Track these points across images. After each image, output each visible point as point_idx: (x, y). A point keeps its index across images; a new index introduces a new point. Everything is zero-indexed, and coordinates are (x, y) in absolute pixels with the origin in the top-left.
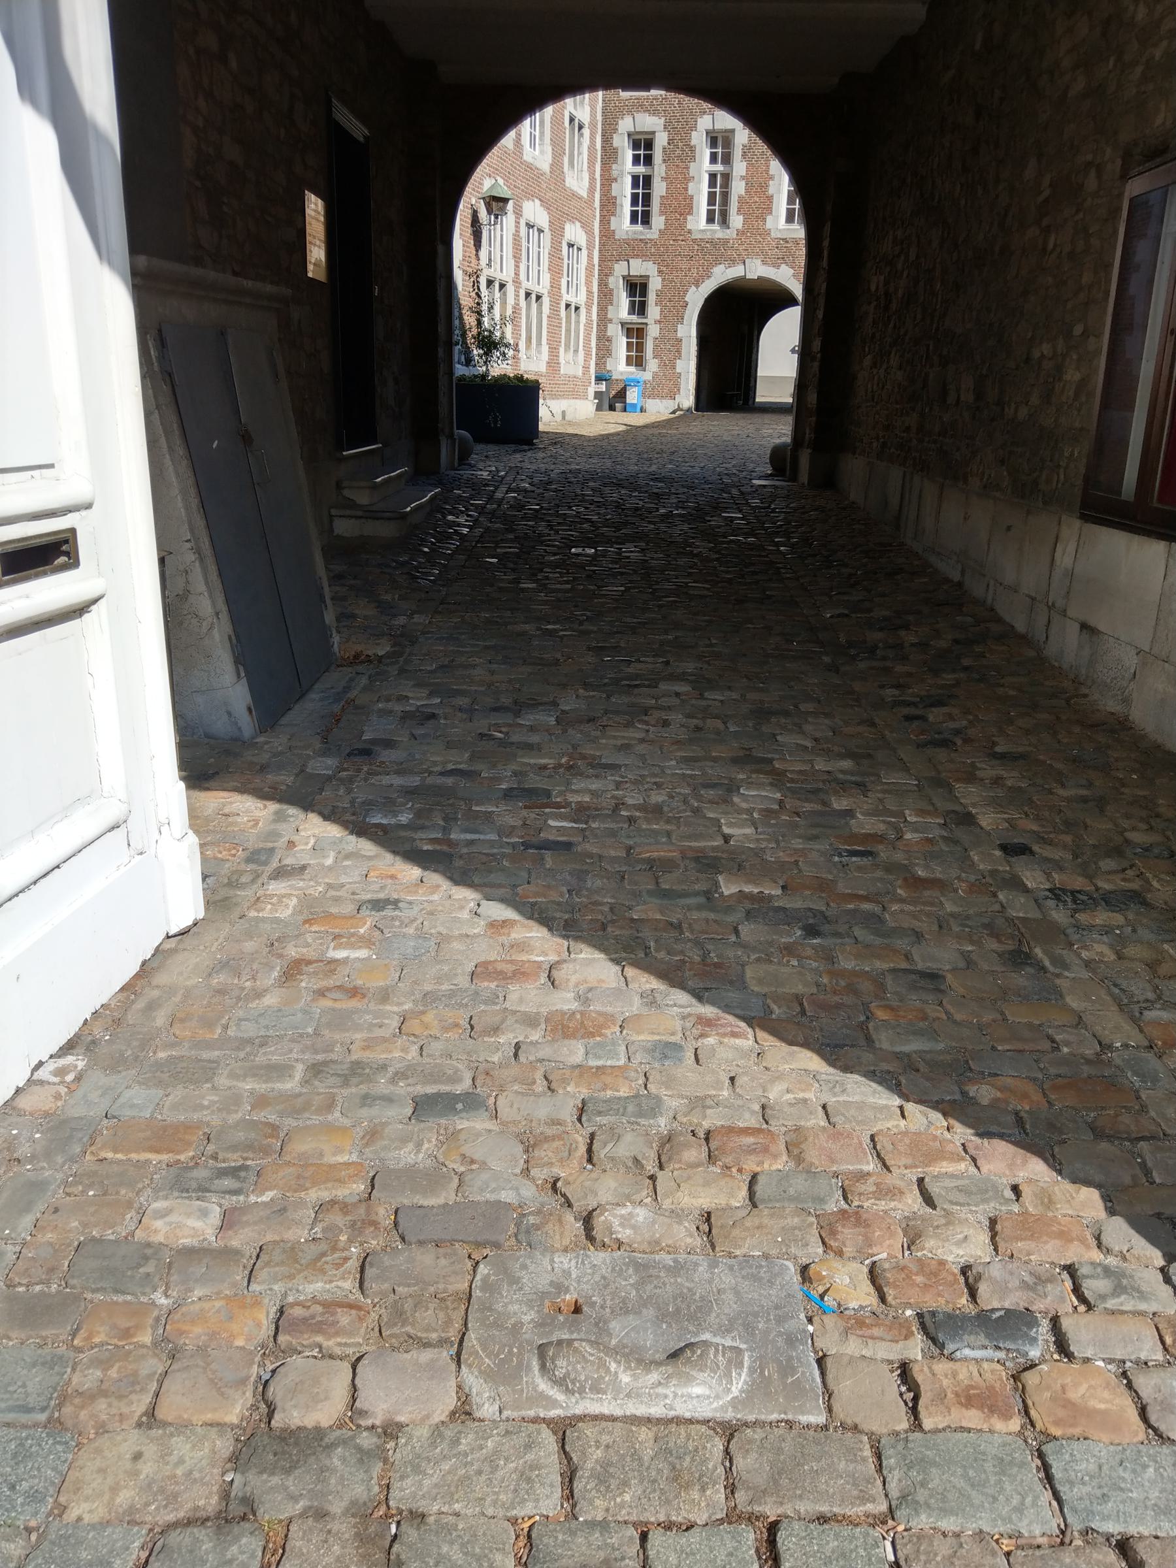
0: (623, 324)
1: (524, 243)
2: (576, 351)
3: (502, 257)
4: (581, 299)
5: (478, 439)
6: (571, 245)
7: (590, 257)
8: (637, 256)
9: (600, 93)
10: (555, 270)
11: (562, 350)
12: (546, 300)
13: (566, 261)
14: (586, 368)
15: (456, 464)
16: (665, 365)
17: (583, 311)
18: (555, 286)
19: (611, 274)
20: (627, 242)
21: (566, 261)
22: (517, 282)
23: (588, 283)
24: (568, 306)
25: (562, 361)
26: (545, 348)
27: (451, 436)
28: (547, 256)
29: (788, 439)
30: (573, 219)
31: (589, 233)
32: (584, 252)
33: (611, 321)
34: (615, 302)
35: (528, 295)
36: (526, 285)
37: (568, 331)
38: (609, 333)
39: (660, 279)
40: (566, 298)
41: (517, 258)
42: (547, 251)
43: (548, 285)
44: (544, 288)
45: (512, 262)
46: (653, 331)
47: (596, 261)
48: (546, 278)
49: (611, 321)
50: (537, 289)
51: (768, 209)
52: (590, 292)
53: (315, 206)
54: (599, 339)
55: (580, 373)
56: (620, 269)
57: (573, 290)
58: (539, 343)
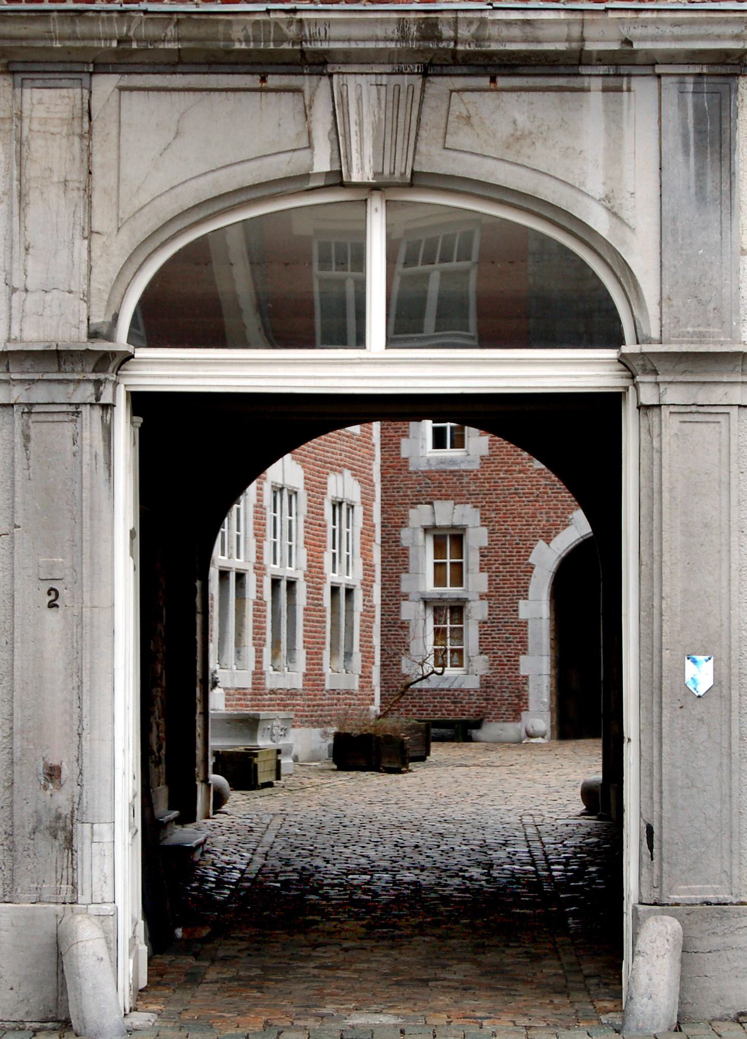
0: (426, 602)
1: (270, 513)
2: (349, 655)
3: (238, 537)
4: (354, 577)
5: (236, 786)
6: (337, 505)
7: (367, 515)
8: (446, 497)
9: (376, 426)
10: (315, 545)
11: (326, 654)
12: (302, 589)
13: (330, 526)
14: (365, 677)
15: (211, 812)
16: (501, 664)
17: (358, 596)
18: (315, 570)
19: (404, 524)
20: (428, 474)
21: (330, 526)
22: (259, 568)
23: (366, 553)
24: (335, 590)
25: (327, 670)
26: (301, 655)
27: (206, 780)
28: (301, 524)
29: (599, 777)
30: (338, 468)
31: (366, 483)
32: (359, 510)
33: (406, 597)
34: (412, 567)
35: (275, 583)
36: (273, 569)
37: (335, 625)
38: (404, 617)
39: (485, 531)
40: (332, 578)
41: (259, 536)
42: (301, 519)
43: (304, 564)
44: (296, 570)
45: (253, 542)
46: (478, 611)
47: (377, 518)
48: (302, 556)
49: (406, 597)
50: (288, 572)
51: (523, 592)
52: (368, 567)
53: (567, 910)
54: (385, 625)
55: (356, 686)
56: (420, 516)
57: (341, 566)
58: (291, 649)
